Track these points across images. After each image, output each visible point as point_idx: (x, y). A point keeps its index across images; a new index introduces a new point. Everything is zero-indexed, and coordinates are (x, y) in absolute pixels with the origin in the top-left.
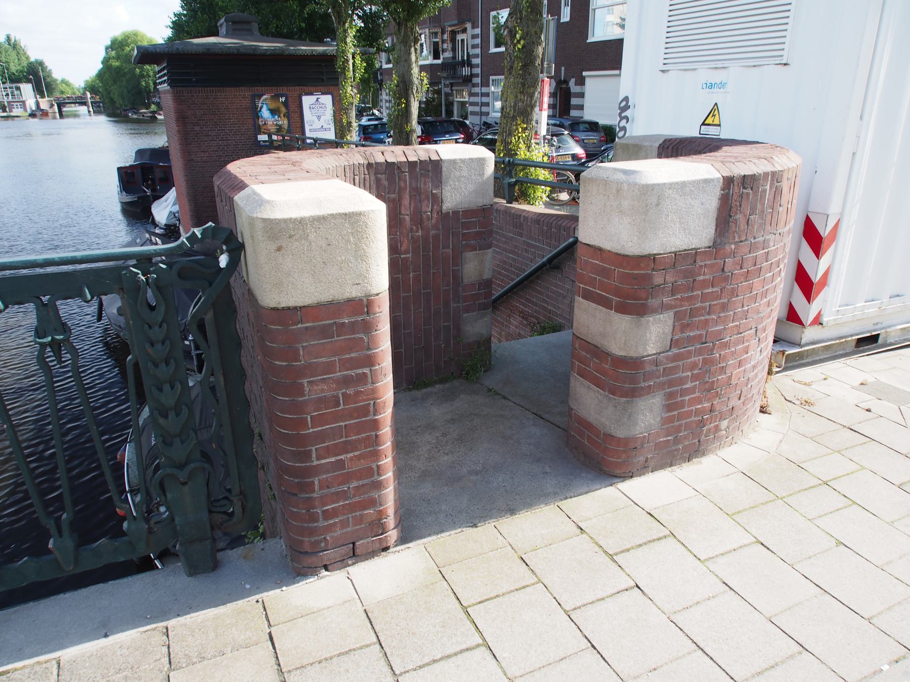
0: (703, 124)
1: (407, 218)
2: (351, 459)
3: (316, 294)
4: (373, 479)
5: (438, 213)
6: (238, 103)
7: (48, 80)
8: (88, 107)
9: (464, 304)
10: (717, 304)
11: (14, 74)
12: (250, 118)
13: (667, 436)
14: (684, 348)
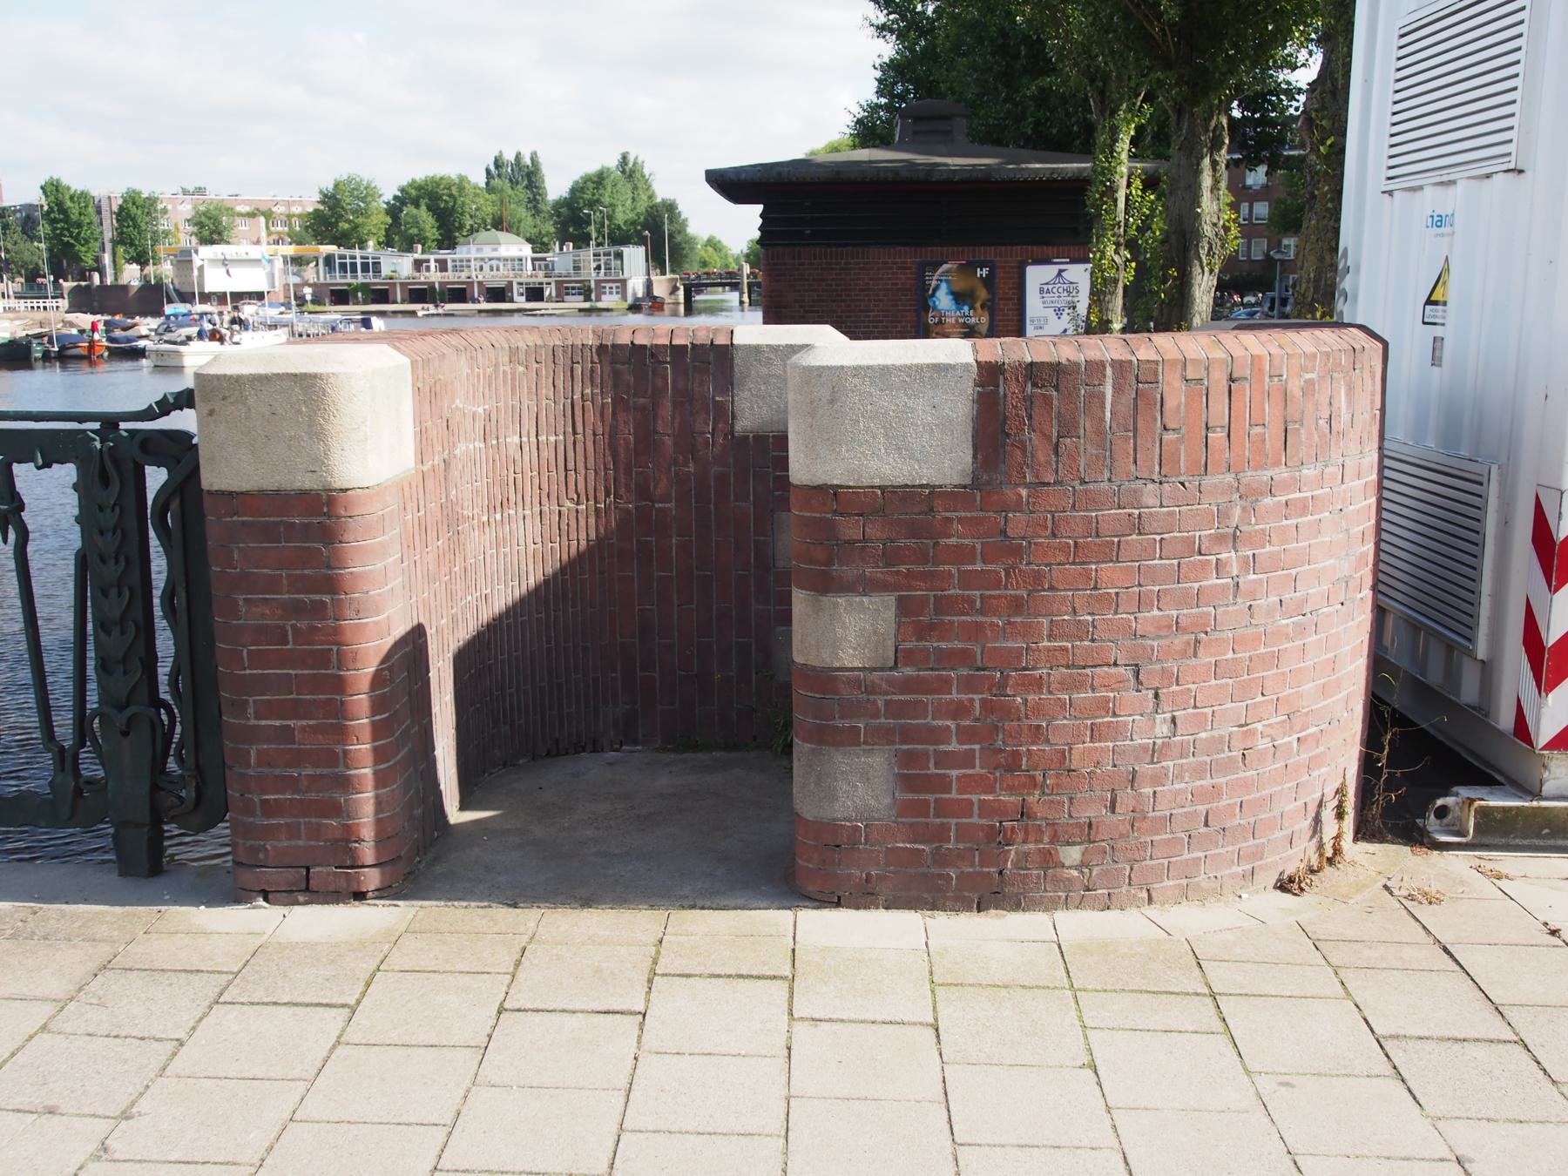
0: (1429, 302)
1: (668, 441)
2: (303, 729)
3: (256, 478)
4: (337, 770)
5: (726, 435)
6: (889, 279)
7: (679, 239)
8: (742, 294)
9: (777, 608)
10: (999, 596)
11: (619, 227)
12: (910, 311)
13: (915, 843)
14: (932, 669)
